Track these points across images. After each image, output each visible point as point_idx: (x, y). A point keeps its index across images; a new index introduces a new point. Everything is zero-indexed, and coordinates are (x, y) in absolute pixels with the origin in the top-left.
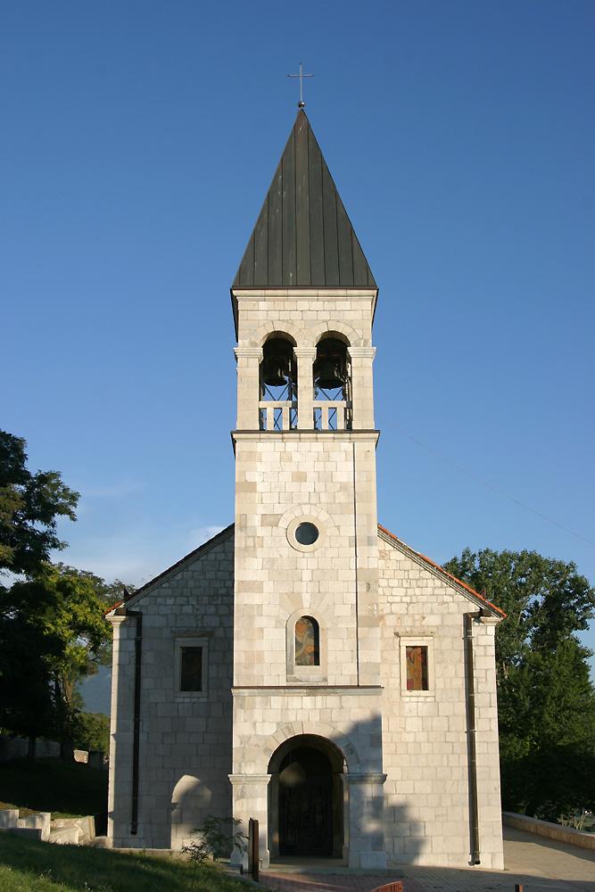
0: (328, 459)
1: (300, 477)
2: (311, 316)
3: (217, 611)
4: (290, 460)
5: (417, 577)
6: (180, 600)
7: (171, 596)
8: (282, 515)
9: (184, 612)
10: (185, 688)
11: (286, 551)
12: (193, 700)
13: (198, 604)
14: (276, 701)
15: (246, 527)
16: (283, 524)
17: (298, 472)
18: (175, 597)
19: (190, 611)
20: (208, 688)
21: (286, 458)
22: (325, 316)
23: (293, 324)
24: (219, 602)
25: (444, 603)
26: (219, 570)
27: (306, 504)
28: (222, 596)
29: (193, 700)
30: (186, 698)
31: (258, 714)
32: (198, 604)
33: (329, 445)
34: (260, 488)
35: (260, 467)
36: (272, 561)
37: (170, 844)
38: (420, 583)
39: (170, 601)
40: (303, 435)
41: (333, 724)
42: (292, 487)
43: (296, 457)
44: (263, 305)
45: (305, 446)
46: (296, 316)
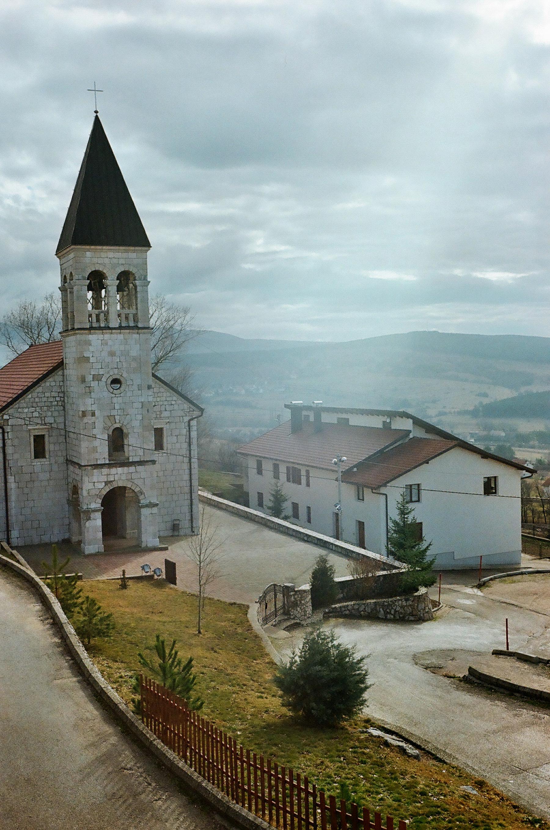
0: (126, 344)
1: (112, 354)
2: (115, 261)
3: (52, 414)
4: (107, 344)
5: (158, 391)
6: (32, 409)
7: (26, 408)
8: (103, 375)
9: (34, 416)
10: (36, 457)
11: (106, 394)
12: (41, 463)
13: (41, 411)
14: (105, 471)
15: (85, 381)
16: (104, 379)
17: (111, 351)
18: (29, 408)
19: (38, 415)
20: (50, 456)
21: (104, 343)
22: (122, 261)
23: (105, 266)
24: (54, 410)
25: (172, 405)
26: (52, 392)
27: (116, 368)
28: (55, 406)
29: (41, 463)
30: (38, 463)
31: (95, 479)
32: (41, 411)
33: (127, 336)
34: (92, 360)
35: (91, 348)
36: (99, 399)
37: (176, 581)
38: (159, 395)
39: (26, 410)
40: (114, 331)
41: (133, 481)
42: (108, 359)
43: (110, 343)
44: (88, 254)
45: (114, 336)
46: (107, 261)
